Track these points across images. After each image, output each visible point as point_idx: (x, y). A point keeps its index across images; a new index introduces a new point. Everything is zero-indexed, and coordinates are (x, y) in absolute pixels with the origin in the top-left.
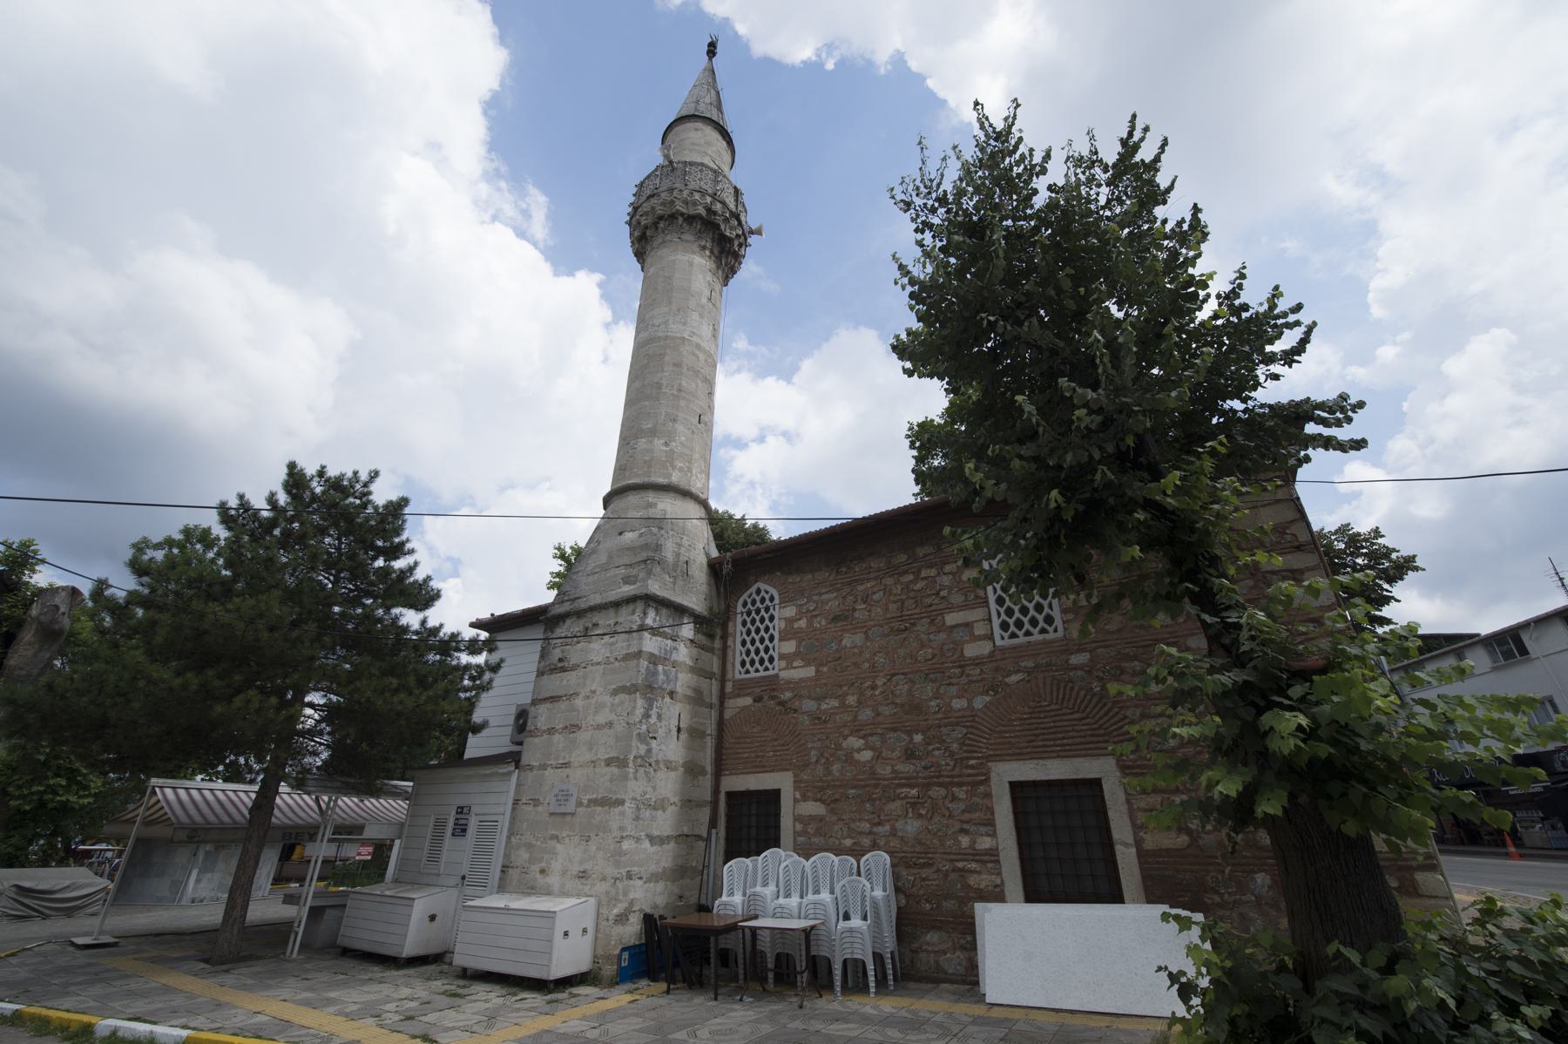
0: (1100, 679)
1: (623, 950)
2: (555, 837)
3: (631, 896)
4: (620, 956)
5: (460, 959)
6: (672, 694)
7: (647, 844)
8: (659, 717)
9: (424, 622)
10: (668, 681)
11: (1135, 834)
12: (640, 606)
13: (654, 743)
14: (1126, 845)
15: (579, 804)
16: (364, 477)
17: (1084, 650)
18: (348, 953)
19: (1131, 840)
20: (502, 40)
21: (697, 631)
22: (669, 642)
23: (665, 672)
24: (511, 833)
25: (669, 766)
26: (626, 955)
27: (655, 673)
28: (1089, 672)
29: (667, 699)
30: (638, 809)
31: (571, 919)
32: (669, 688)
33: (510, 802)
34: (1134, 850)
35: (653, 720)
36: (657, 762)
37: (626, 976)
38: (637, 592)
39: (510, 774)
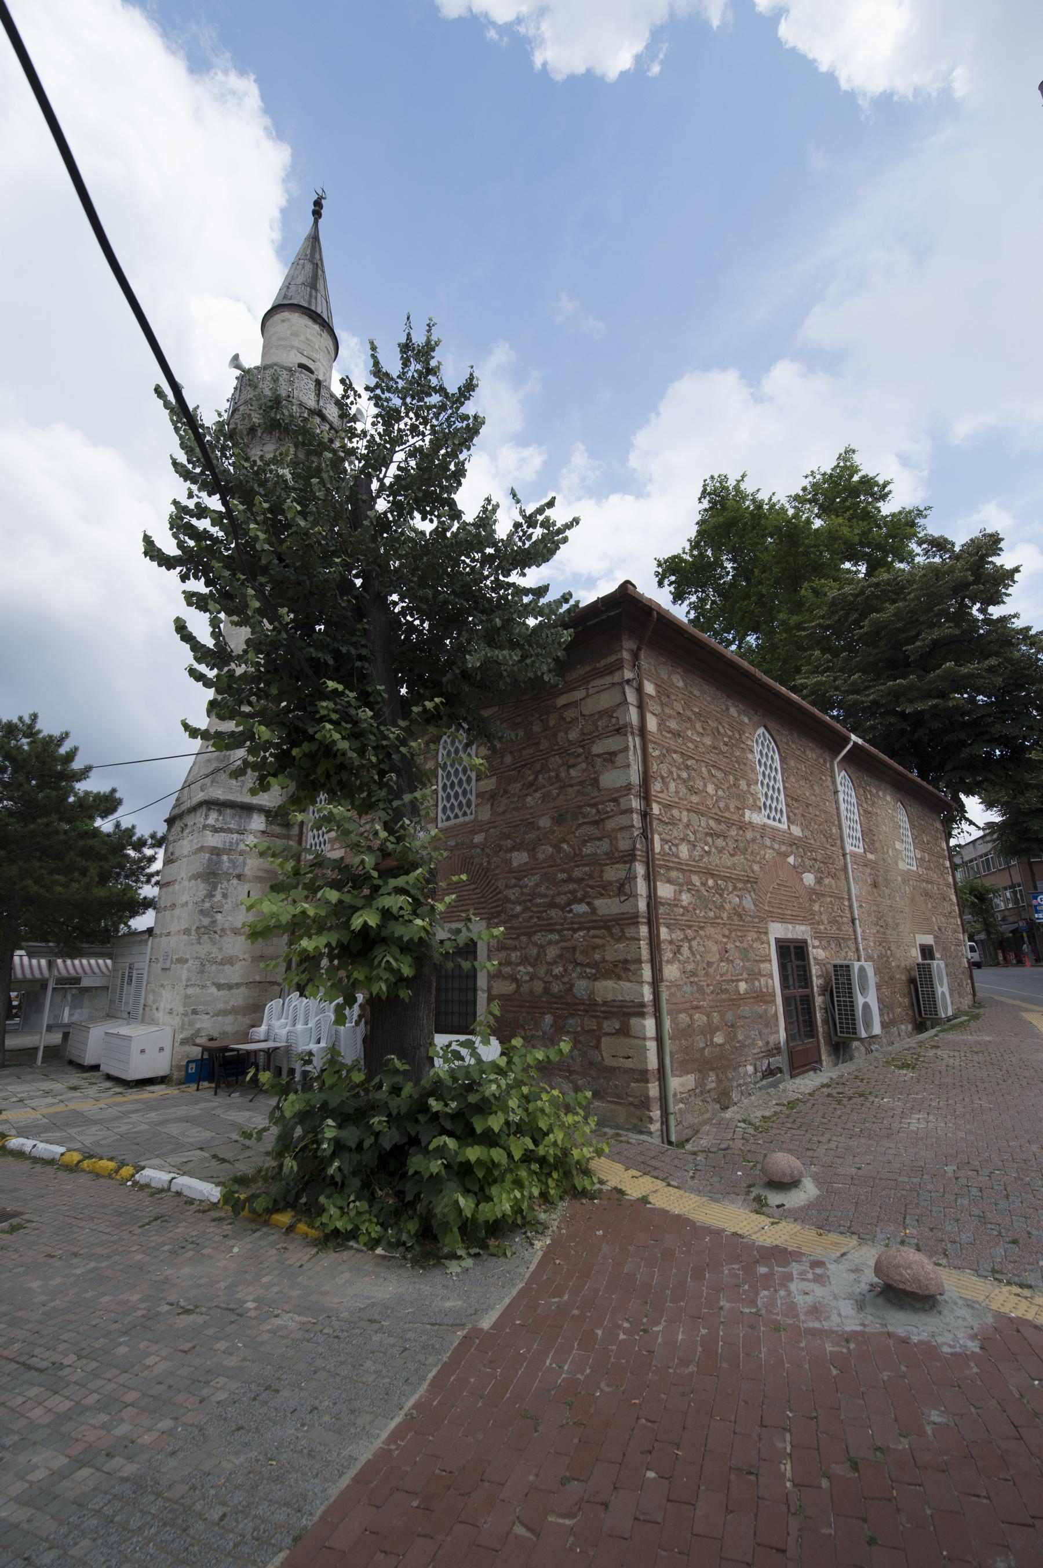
0: (488, 855)
1: (189, 1062)
2: (162, 985)
3: (198, 1026)
4: (187, 1066)
5: (104, 1068)
6: (239, 877)
7: (214, 990)
8: (225, 896)
9: (118, 825)
10: (235, 867)
11: (489, 982)
12: (204, 809)
13: (219, 916)
14: (483, 991)
15: (172, 962)
16: (27, 721)
17: (481, 831)
18: (71, 1063)
19: (485, 988)
20: (279, 131)
21: (269, 823)
22: (235, 836)
23: (230, 860)
24: (148, 983)
25: (236, 932)
26: (193, 1065)
27: (219, 862)
28: (483, 849)
29: (235, 881)
30: (202, 964)
31: (150, 1040)
32: (236, 872)
33: (148, 960)
34: (486, 995)
35: (218, 897)
36: (223, 930)
37: (188, 1079)
38: (206, 798)
39: (147, 941)
